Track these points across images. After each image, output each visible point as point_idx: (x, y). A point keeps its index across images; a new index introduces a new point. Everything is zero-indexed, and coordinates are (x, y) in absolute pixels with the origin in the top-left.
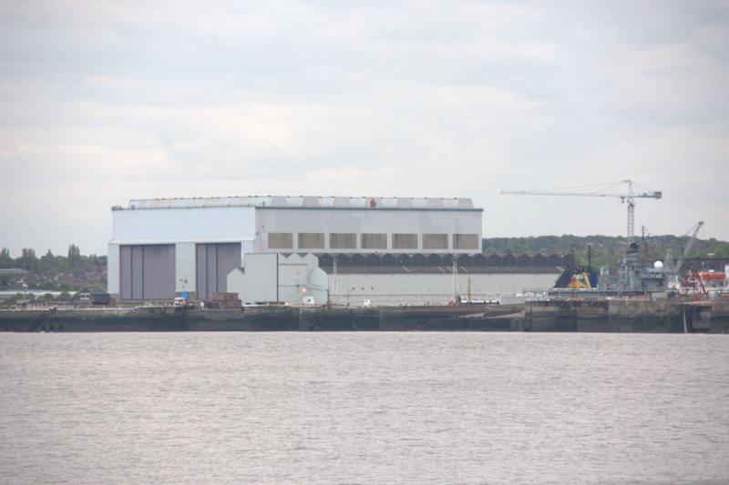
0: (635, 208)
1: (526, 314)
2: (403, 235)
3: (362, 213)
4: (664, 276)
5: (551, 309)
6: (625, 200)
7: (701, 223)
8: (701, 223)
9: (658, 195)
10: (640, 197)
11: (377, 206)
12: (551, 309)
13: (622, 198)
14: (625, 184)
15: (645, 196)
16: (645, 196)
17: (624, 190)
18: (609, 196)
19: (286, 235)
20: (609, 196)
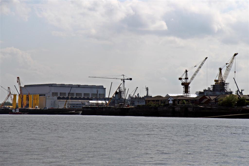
0: (125, 82)
1: (215, 99)
2: (86, 94)
3: (76, 88)
4: (125, 101)
5: (89, 109)
6: (122, 80)
7: (137, 87)
8: (137, 87)
9: (131, 79)
10: (126, 79)
11: (80, 87)
12: (89, 109)
13: (122, 79)
14: (122, 76)
15: (127, 79)
16: (127, 79)
17: (122, 77)
18: (118, 79)
19: (56, 93)
20: (118, 79)
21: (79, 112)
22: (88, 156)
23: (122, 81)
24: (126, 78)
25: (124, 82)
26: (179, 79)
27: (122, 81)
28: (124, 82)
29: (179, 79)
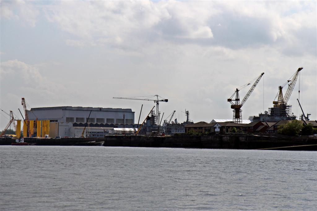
0: (159, 105)
1: (274, 126)
2: (109, 119)
3: (97, 112)
4: (159, 128)
5: (114, 139)
6: (156, 102)
7: (175, 111)
8: (175, 111)
9: (167, 101)
10: (160, 101)
11: (102, 110)
12: (114, 139)
13: (155, 101)
14: (156, 96)
15: (162, 101)
16: (162, 101)
17: (156, 98)
18: (150, 100)
19: (72, 118)
20: (150, 100)
21: (100, 143)
22: (111, 198)
23: (155, 102)
24: (160, 99)
25: (158, 104)
26: (228, 101)
27: (155, 102)
28: (158, 104)
29: (228, 101)
